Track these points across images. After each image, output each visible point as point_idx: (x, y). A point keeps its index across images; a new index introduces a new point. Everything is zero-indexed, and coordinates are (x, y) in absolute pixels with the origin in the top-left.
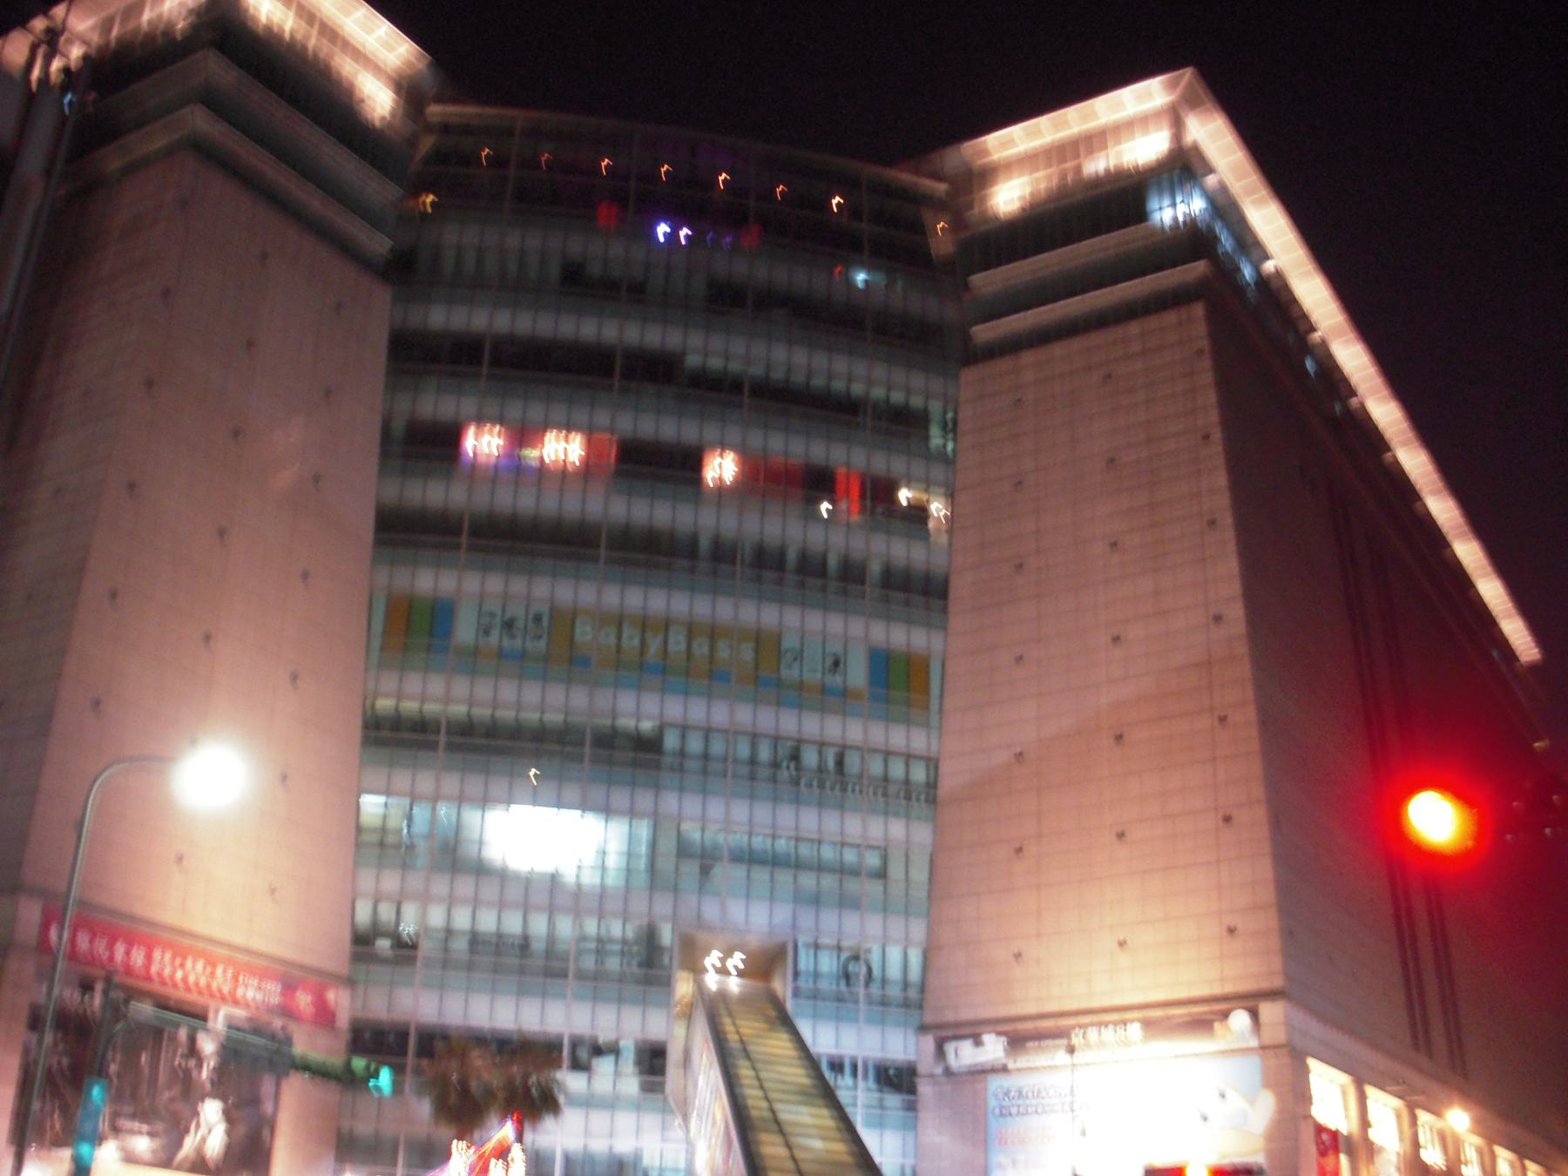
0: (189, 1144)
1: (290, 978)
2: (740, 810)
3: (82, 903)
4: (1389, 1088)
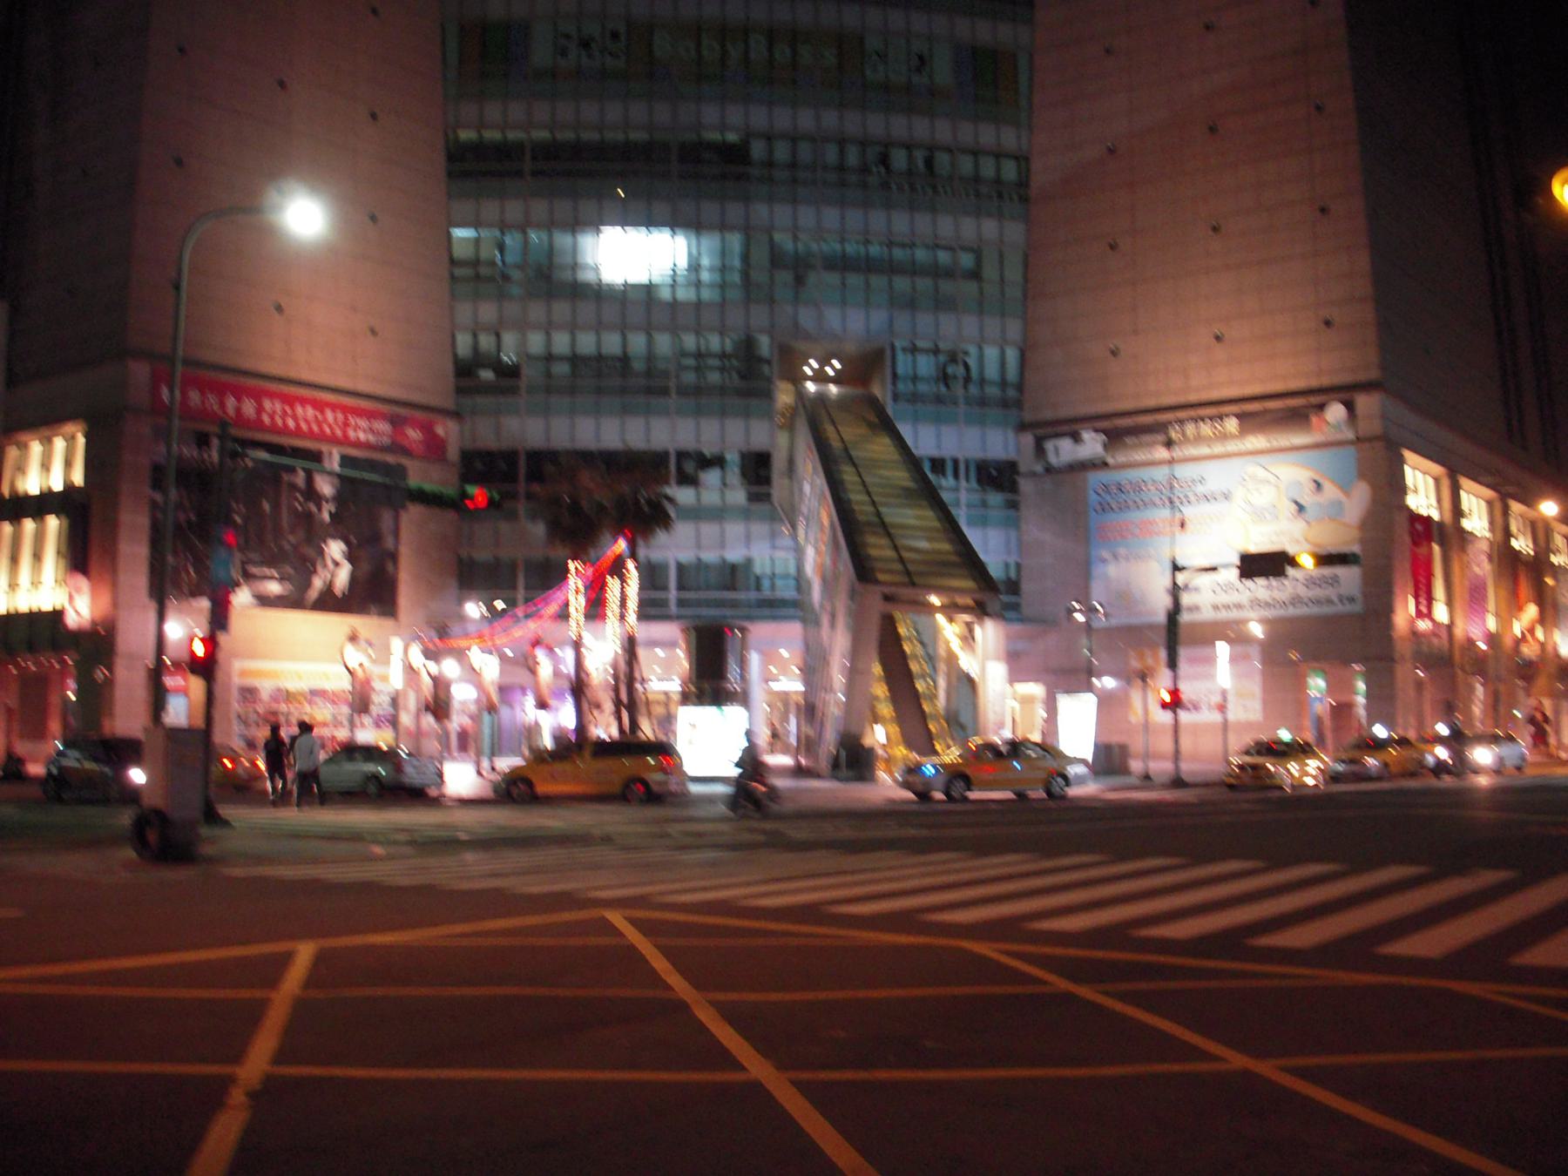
0: (318, 583)
1: (397, 412)
2: (831, 215)
3: (187, 362)
4: (1481, 479)
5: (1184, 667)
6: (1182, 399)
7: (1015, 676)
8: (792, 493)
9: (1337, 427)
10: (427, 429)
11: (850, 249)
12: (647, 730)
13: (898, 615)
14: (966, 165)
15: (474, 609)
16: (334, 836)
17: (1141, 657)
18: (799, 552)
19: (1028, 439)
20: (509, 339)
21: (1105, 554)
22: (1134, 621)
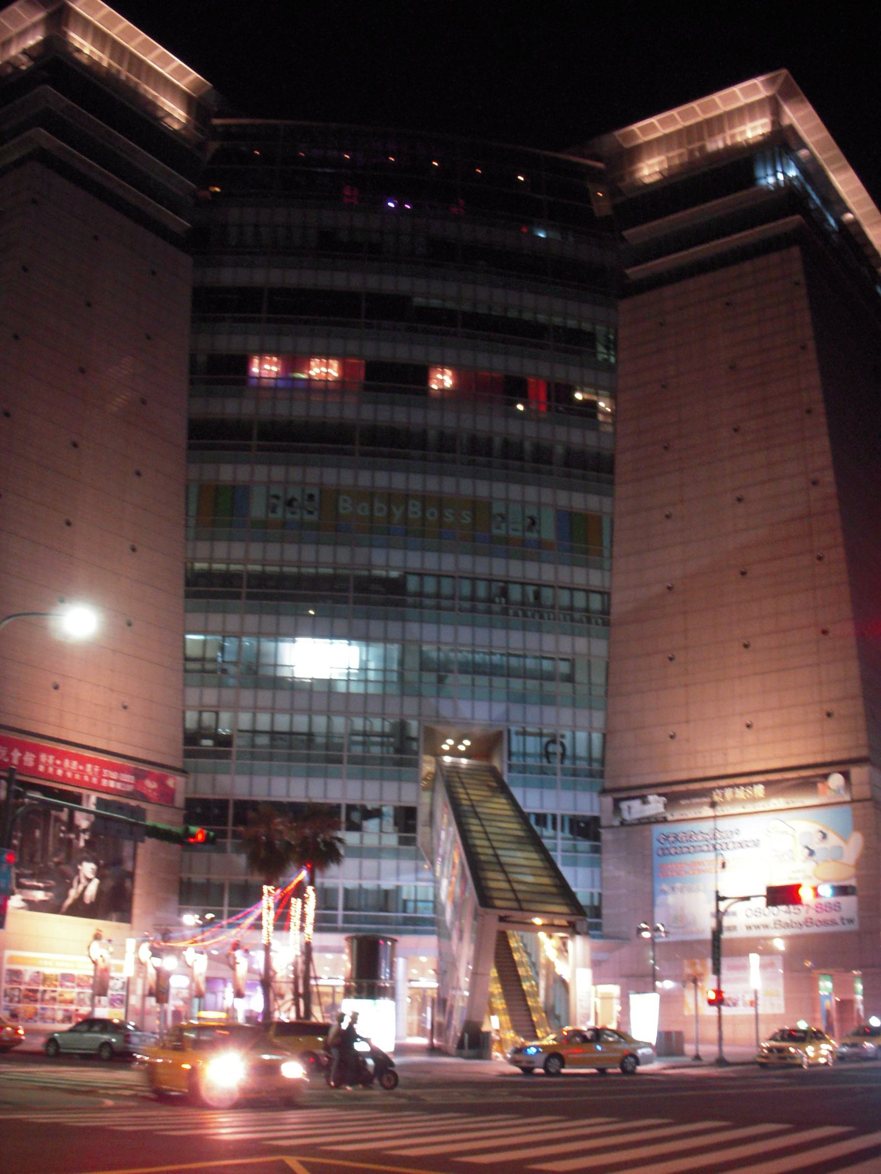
0: (73, 894)
2: (465, 633)
5: (725, 973)
6: (722, 772)
7: (598, 980)
8: (432, 838)
9: (837, 792)
10: (161, 780)
11: (478, 658)
12: (318, 1016)
13: (510, 932)
15: (190, 919)
16: (73, 1091)
17: (693, 965)
18: (436, 882)
19: (608, 801)
20: (225, 717)
21: (665, 887)
22: (688, 938)
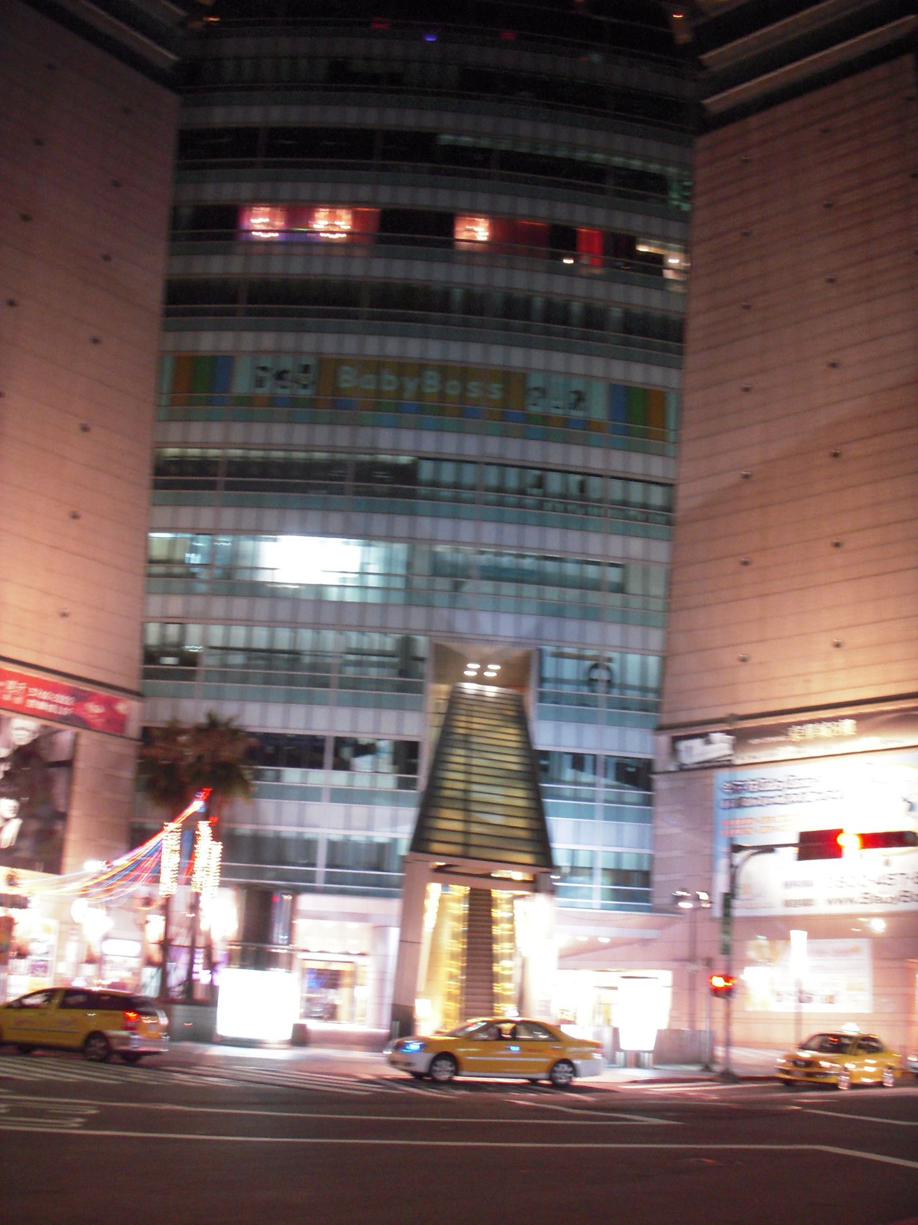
2: (489, 531)
10: (109, 703)
14: (368, 382)
19: (664, 739)
20: (194, 630)
